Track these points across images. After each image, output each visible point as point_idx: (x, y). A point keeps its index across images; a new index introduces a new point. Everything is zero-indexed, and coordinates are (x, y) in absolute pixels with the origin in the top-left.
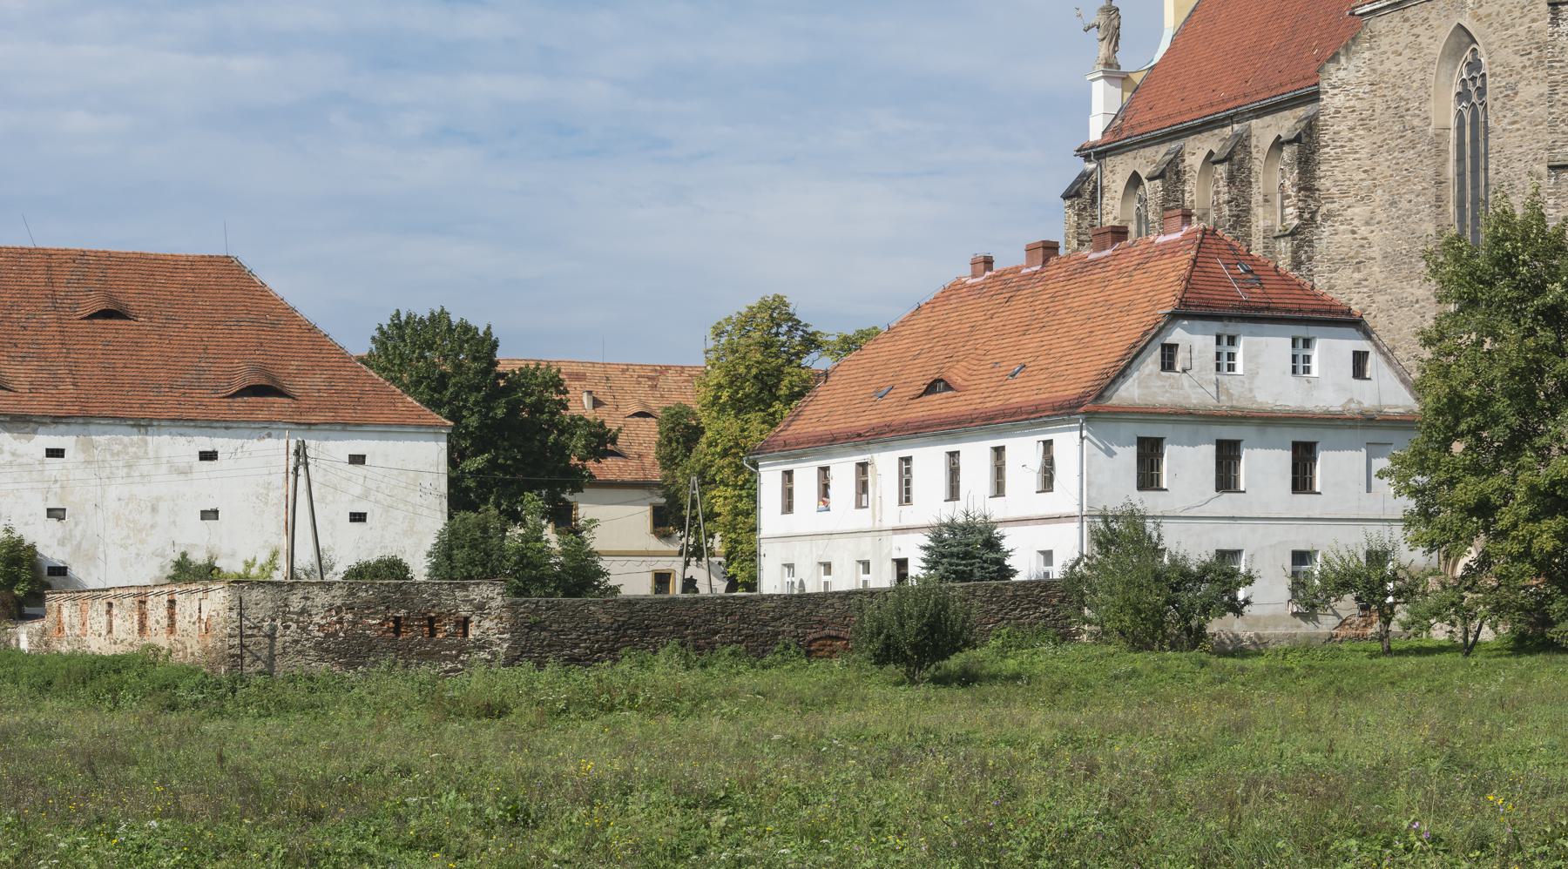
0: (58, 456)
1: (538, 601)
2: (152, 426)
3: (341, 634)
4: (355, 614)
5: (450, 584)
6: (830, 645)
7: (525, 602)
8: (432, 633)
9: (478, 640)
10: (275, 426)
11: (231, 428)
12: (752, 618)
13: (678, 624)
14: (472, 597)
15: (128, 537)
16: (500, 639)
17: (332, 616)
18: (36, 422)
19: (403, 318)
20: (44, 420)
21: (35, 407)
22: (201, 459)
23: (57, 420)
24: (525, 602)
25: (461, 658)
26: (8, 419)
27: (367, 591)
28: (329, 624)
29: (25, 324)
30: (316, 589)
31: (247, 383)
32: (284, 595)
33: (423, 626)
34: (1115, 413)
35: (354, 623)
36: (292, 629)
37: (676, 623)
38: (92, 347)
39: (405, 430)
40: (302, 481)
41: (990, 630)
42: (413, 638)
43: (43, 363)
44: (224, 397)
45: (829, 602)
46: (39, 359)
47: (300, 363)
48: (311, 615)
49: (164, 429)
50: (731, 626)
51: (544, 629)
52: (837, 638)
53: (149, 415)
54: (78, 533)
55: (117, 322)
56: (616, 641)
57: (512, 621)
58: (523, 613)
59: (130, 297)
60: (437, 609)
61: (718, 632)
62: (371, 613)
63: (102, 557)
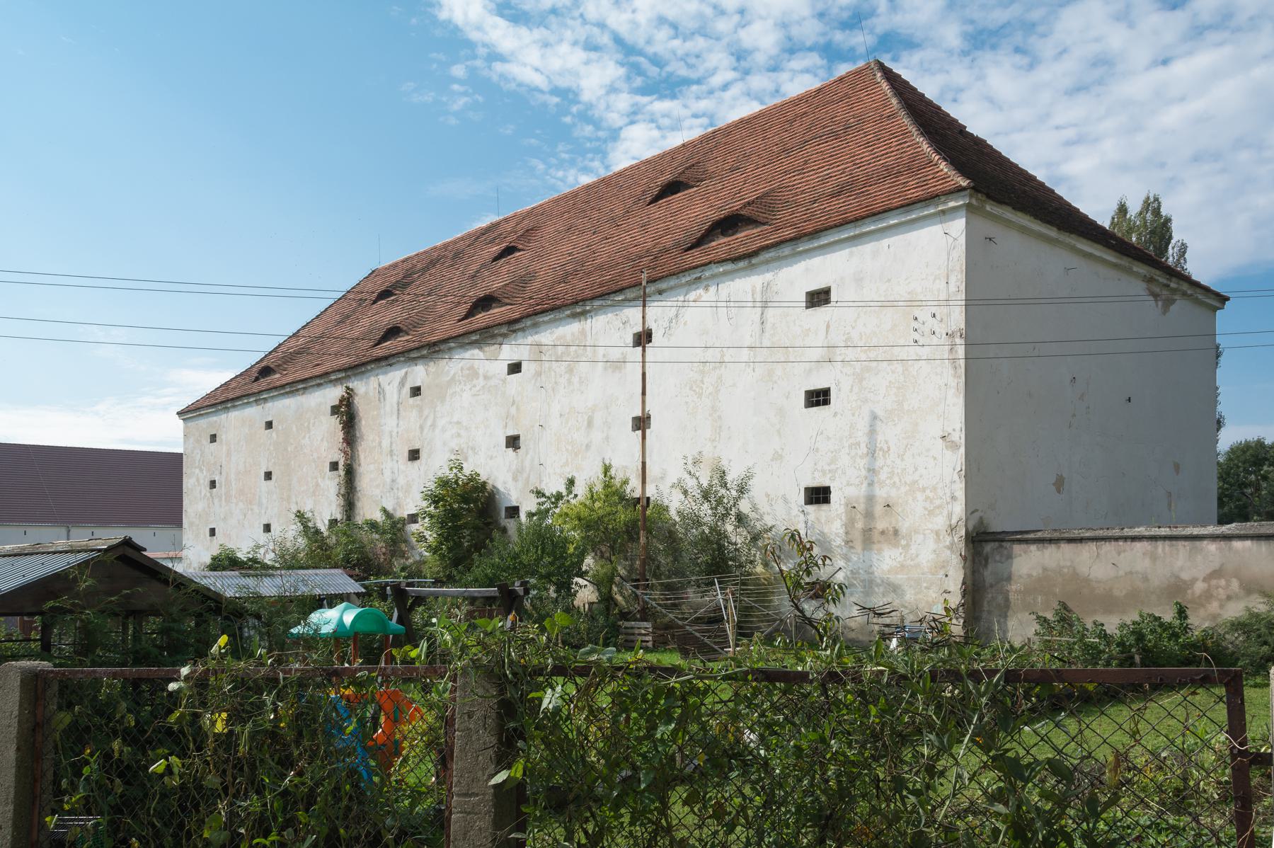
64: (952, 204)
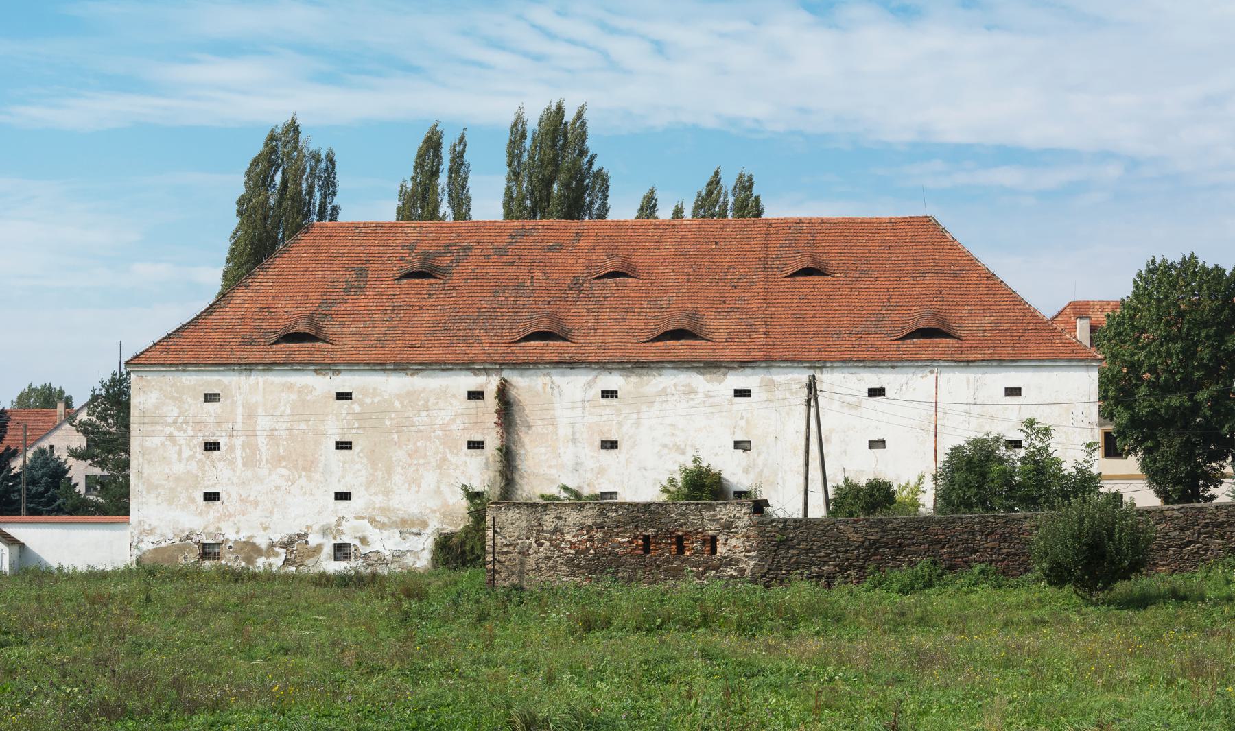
0: (745, 396)
2: (826, 367)
3: (592, 552)
5: (698, 504)
8: (681, 550)
9: (727, 557)
10: (936, 364)
12: (1014, 537)
13: (932, 543)
14: (719, 517)
16: (747, 557)
17: (583, 535)
18: (725, 367)
19: (1158, 262)
20: (732, 365)
21: (726, 354)
22: (870, 395)
23: (743, 364)
26: (702, 365)
27: (617, 511)
28: (581, 541)
29: (736, 284)
30: (568, 510)
31: (917, 327)
32: (538, 515)
33: (671, 544)
35: (604, 541)
36: (545, 546)
37: (932, 542)
38: (790, 301)
39: (1058, 364)
40: (813, 411)
43: (744, 317)
44: (895, 340)
46: (742, 312)
47: (973, 307)
48: (563, 534)
49: (835, 370)
50: (991, 545)
51: (793, 547)
53: (823, 357)
55: (817, 278)
56: (867, 559)
57: (759, 539)
58: (771, 532)
59: (831, 255)
61: (977, 551)
62: (620, 532)
63: (781, 482)
64: (1094, 364)
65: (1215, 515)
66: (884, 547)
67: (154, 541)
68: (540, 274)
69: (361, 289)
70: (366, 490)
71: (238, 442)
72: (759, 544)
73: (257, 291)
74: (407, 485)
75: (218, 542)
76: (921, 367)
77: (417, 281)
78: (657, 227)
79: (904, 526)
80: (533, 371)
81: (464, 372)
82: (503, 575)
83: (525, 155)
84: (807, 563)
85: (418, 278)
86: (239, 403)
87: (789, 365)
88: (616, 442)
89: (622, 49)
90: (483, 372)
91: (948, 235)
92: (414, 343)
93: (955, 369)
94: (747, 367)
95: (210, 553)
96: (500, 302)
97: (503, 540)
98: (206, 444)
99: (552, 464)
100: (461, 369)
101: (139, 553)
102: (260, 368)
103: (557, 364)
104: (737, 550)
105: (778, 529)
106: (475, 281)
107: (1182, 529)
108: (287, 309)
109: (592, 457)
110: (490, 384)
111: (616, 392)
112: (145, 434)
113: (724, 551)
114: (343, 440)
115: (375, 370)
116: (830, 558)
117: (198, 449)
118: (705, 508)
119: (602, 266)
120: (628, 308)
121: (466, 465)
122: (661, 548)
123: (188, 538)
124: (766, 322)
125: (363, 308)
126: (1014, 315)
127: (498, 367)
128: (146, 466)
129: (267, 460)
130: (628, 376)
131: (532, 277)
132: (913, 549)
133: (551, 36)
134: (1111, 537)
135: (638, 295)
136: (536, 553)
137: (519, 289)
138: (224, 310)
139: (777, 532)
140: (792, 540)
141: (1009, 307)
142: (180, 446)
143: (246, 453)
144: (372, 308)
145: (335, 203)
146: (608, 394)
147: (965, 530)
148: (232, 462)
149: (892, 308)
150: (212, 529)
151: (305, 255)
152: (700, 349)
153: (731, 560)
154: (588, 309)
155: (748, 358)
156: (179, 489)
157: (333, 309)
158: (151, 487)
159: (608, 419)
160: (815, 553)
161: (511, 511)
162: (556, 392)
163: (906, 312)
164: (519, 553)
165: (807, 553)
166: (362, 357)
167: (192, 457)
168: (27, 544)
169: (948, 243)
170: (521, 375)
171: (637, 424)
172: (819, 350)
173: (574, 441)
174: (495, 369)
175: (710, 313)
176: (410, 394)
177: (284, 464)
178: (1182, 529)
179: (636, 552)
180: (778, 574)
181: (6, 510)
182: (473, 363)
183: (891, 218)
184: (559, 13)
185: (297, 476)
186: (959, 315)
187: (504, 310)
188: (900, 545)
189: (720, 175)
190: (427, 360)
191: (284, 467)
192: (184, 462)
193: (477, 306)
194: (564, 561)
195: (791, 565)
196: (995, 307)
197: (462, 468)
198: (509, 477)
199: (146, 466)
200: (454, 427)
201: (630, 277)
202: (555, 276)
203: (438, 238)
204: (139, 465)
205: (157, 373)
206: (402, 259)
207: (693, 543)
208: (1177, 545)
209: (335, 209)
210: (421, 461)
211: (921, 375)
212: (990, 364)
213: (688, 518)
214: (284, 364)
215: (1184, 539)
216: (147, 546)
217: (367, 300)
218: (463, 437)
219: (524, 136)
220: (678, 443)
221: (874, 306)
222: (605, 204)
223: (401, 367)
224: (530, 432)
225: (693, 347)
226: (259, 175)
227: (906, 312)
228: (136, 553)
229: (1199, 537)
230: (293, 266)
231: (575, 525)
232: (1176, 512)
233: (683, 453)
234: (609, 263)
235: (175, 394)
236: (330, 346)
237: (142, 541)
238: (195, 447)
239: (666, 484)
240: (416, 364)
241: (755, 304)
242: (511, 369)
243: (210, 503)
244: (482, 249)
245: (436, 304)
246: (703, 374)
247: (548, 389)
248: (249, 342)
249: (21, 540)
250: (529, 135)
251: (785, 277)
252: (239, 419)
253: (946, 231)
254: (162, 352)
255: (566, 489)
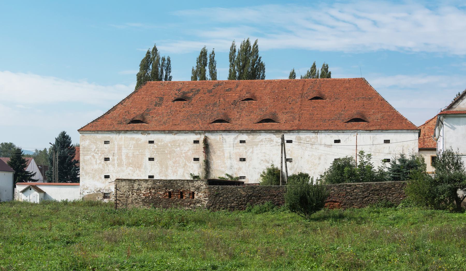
1: (219, 187)
2: (319, 132)
3: (151, 197)
4: (155, 190)
6: (333, 204)
7: (214, 187)
8: (182, 197)
9: (197, 200)
10: (358, 131)
11: (344, 132)
13: (271, 196)
14: (195, 185)
15: (311, 167)
16: (205, 200)
17: (148, 191)
20: (286, 132)
21: (283, 127)
24: (214, 187)
25: (191, 206)
26: (275, 131)
30: (143, 182)
32: (132, 184)
33: (178, 195)
34: (457, 114)
35: (155, 193)
36: (134, 195)
37: (271, 195)
41: (401, 200)
42: (175, 199)
43: (292, 114)
44: (345, 123)
45: (332, 188)
46: (291, 113)
47: (375, 111)
48: (141, 190)
49: (322, 133)
51: (221, 196)
52: (335, 202)
53: (318, 129)
54: (296, 166)
55: (320, 100)
56: (247, 201)
57: (209, 193)
58: (213, 191)
60: (183, 189)
62: (161, 190)
64: (416, 131)
65: (375, 186)
66: (254, 197)
67: (88, 192)
68: (222, 99)
69: (160, 105)
70: (159, 175)
71: (116, 158)
72: (209, 195)
73: (125, 106)
74: (173, 173)
75: (109, 192)
76: (353, 132)
77: (180, 102)
78: (265, 82)
79: (261, 189)
80: (216, 134)
81: (192, 134)
82: (120, 205)
83: (236, 57)
84: (226, 202)
85: (180, 101)
86: (116, 144)
87: (306, 131)
88: (245, 159)
89: (361, 23)
90: (199, 134)
91: (368, 84)
92: (176, 123)
93: (366, 133)
94: (291, 132)
95: (107, 197)
96: (207, 109)
97: (120, 193)
98: (105, 158)
99: (223, 166)
100: (191, 133)
101: (83, 196)
102: (123, 132)
103: (224, 131)
104: (201, 197)
105: (215, 190)
106: (200, 102)
107: (363, 192)
108: (134, 112)
109: (237, 164)
110: (201, 138)
111: (245, 141)
112: (85, 155)
113: (197, 197)
114: (151, 157)
115: (162, 133)
116: (235, 201)
117: (102, 160)
118: (190, 182)
119: (244, 96)
120: (251, 111)
121: (193, 167)
122: (175, 196)
123: (99, 191)
124: (299, 116)
125: (160, 111)
126: (389, 113)
127: (204, 132)
128: (85, 166)
129: (125, 164)
130: (249, 135)
131: (220, 100)
132: (264, 198)
133: (338, 20)
134: (309, 195)
135: (256, 107)
136: (131, 197)
137: (214, 105)
138: (113, 112)
139: (215, 191)
140: (221, 194)
141: (388, 111)
142: (96, 159)
143: (118, 162)
144: (163, 111)
145: (170, 75)
146: (242, 142)
147: (283, 191)
148: (114, 165)
149: (345, 111)
150: (107, 188)
151: (143, 93)
152: (275, 126)
153: (199, 201)
154: (238, 112)
155: (291, 129)
156: (96, 174)
157: (150, 112)
158: (87, 174)
159: (242, 151)
160: (229, 199)
161: (123, 182)
162: (224, 141)
163: (350, 112)
164: (126, 197)
165: (227, 199)
166: (157, 128)
167: (100, 163)
168: (47, 192)
169: (369, 88)
170: (212, 135)
171: (252, 152)
172: (317, 126)
173: (230, 158)
174: (203, 133)
175: (280, 113)
176: (174, 141)
177: (131, 166)
178: (363, 192)
179: (166, 197)
180: (216, 206)
181: (75, 181)
182: (195, 131)
183: (349, 79)
184: (340, 11)
185: (135, 170)
186: (369, 113)
187: (208, 112)
188: (260, 196)
189: (316, 64)
190: (179, 129)
191: (131, 167)
192: (98, 165)
193: (199, 111)
194: (141, 200)
195: (220, 203)
196: (383, 111)
197: (192, 167)
198: (208, 170)
199: (85, 166)
200: (189, 153)
201: (253, 100)
202: (227, 100)
203: (189, 87)
204: (83, 166)
205: (89, 134)
206: (176, 94)
207: (186, 194)
208: (361, 198)
209: (171, 77)
210: (178, 165)
211: (353, 135)
212: (378, 131)
213: (184, 186)
214: (131, 131)
215: (363, 195)
216: (86, 193)
217: (162, 109)
218: (192, 157)
219: (235, 51)
220: (267, 159)
221: (339, 110)
222: (264, 74)
223: (170, 132)
224: (215, 155)
225: (273, 125)
226: (144, 65)
227: (350, 112)
228: (82, 196)
229: (369, 195)
230: (138, 97)
231: (145, 187)
232: (361, 186)
233: (269, 163)
234: (247, 95)
235: (95, 141)
236: (147, 125)
237: (84, 192)
238: (101, 160)
239: (262, 173)
240: (175, 131)
241: (296, 110)
242: (208, 133)
243: (107, 179)
244: (204, 91)
245: (185, 110)
246: (274, 134)
247: (221, 140)
248: (121, 123)
249: (45, 191)
250: (237, 51)
251: (309, 100)
252: (116, 149)
253: (368, 83)
254: (91, 127)
255: (227, 175)
